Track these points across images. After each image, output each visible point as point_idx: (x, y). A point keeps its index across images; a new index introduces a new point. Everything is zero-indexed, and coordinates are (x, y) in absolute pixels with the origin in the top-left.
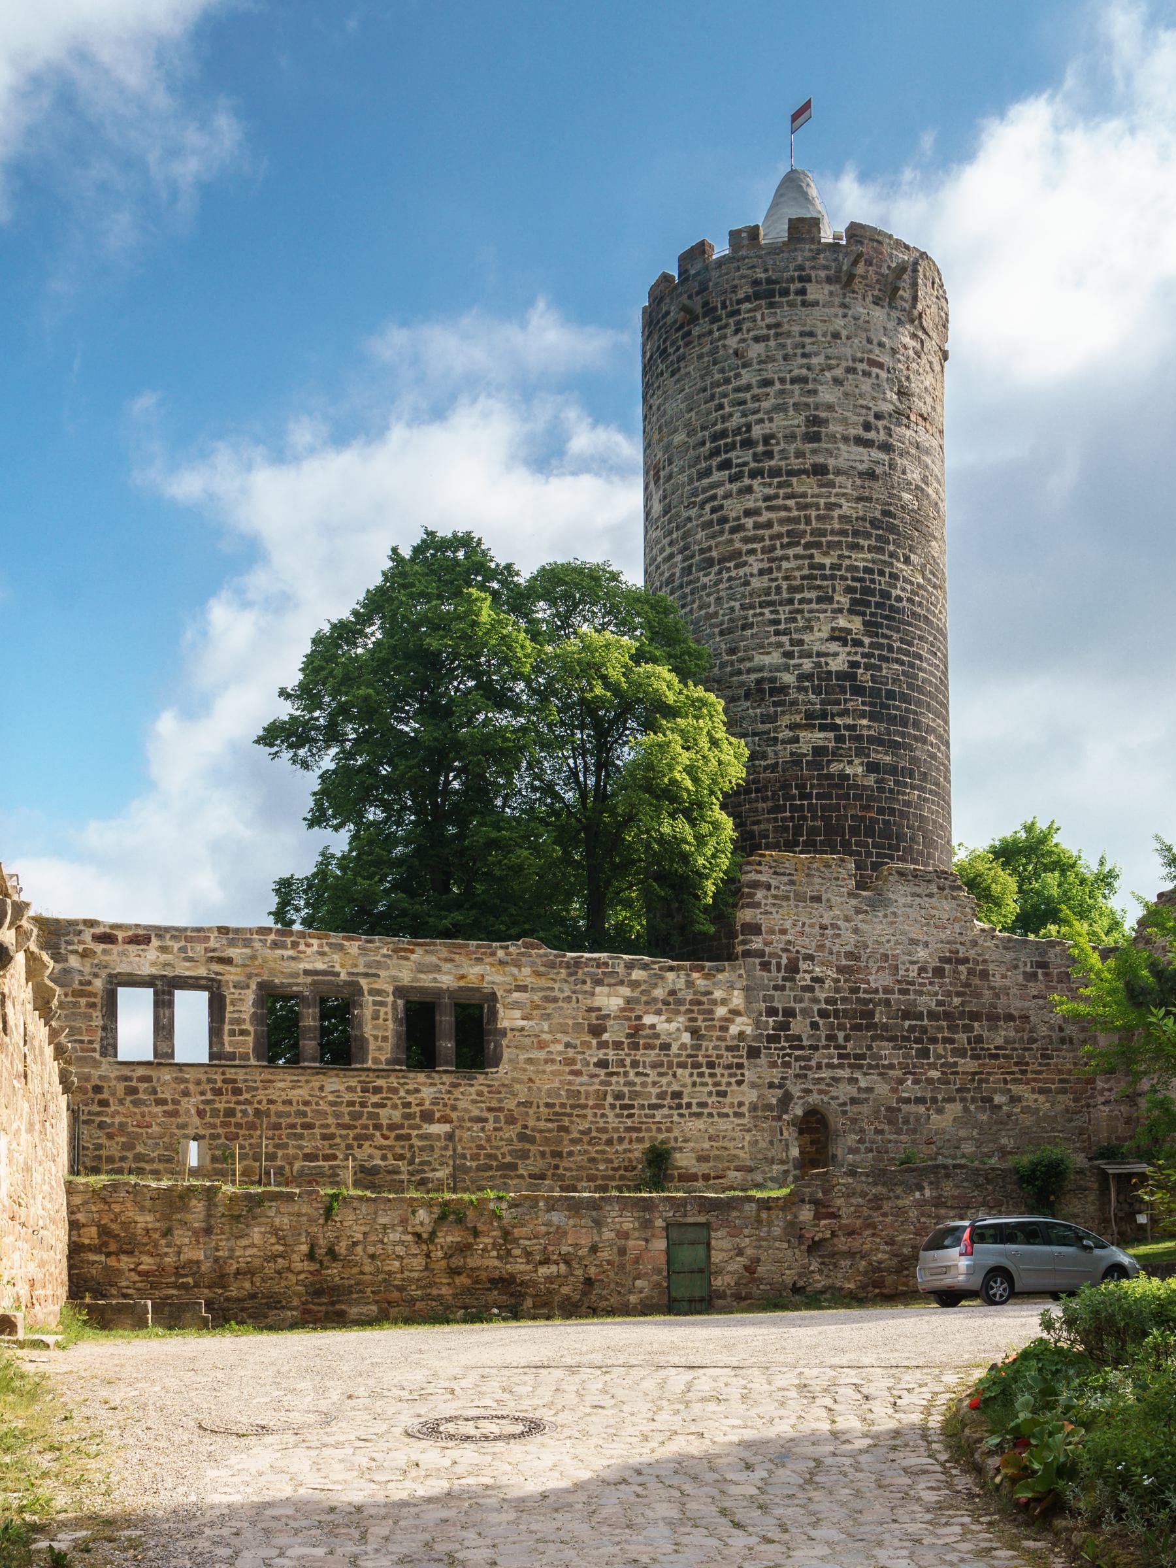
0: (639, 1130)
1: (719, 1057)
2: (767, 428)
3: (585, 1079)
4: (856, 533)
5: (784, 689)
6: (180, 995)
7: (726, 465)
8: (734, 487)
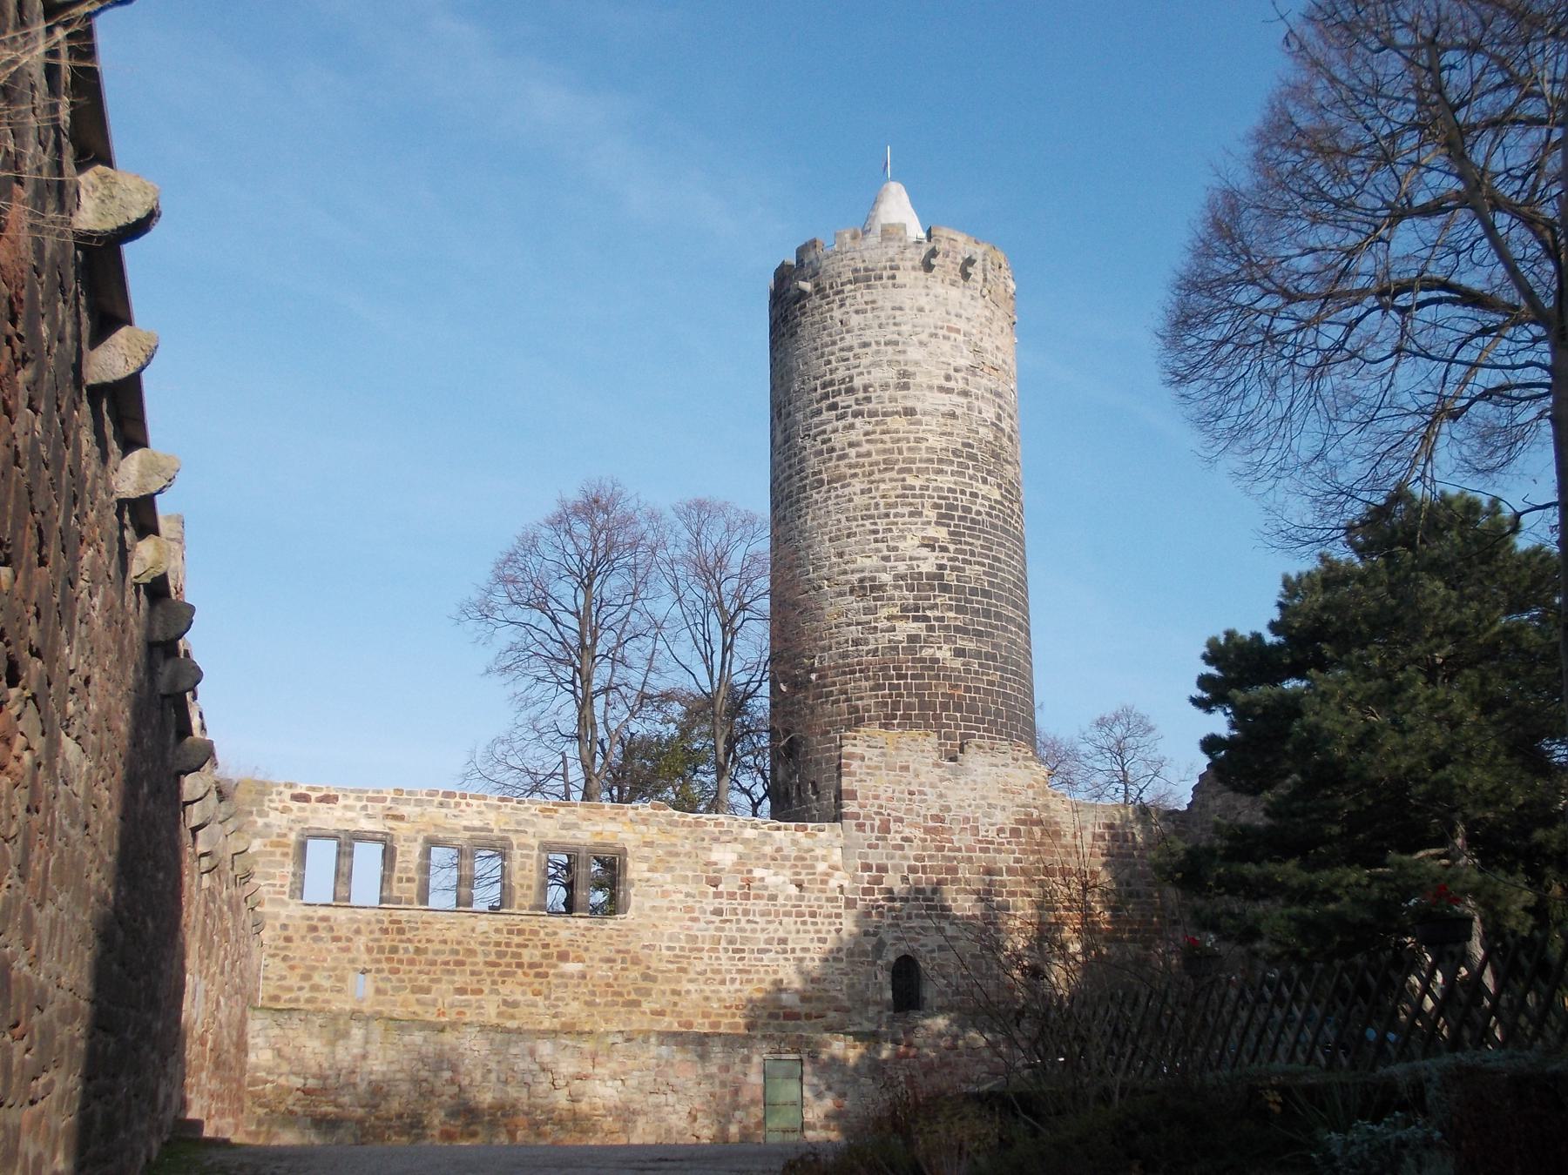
0: (748, 972)
1: (820, 907)
2: (865, 379)
3: (702, 925)
4: (940, 461)
5: (881, 587)
6: (359, 847)
7: (834, 407)
8: (840, 424)
